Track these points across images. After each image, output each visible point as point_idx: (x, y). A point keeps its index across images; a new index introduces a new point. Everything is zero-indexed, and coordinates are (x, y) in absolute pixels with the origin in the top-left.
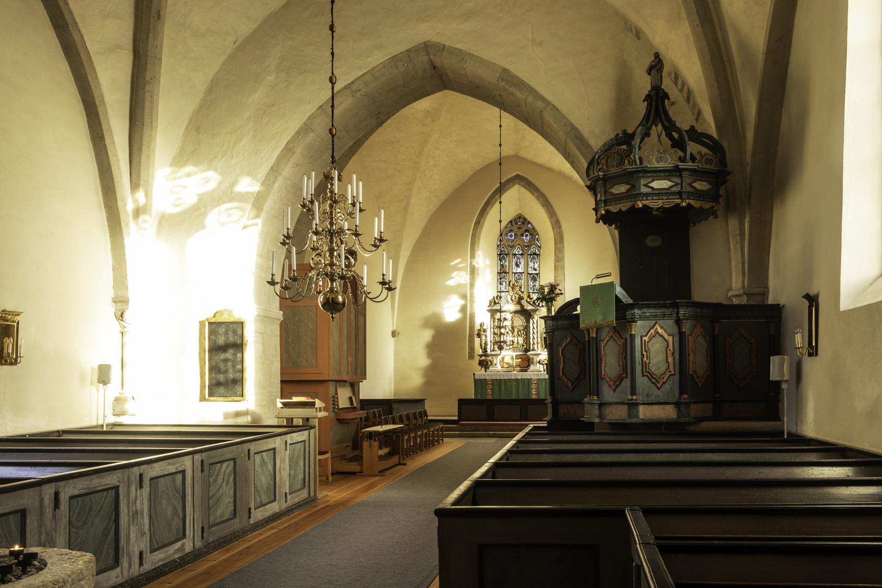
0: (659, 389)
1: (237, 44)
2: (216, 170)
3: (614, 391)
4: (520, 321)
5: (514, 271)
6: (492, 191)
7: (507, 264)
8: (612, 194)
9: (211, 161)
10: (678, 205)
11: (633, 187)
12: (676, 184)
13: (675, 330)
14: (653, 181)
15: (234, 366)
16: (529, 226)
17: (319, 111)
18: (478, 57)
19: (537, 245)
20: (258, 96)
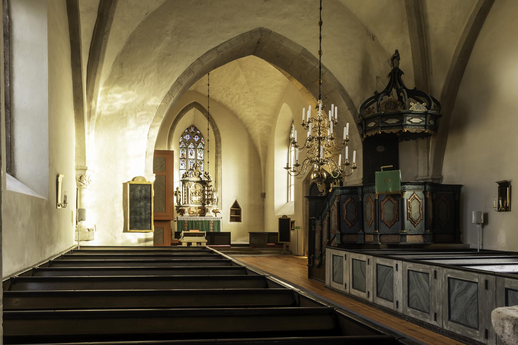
0: (415, 227)
1: (148, 15)
2: (134, 91)
3: (390, 228)
4: (199, 187)
5: (189, 158)
6: (180, 111)
7: (185, 153)
8: (387, 123)
9: (130, 85)
10: (423, 132)
11: (402, 121)
12: (423, 121)
13: (423, 196)
14: (412, 118)
15: (145, 211)
16: (198, 132)
17: (198, 61)
18: (289, 40)
19: (202, 143)
20: (160, 48)
